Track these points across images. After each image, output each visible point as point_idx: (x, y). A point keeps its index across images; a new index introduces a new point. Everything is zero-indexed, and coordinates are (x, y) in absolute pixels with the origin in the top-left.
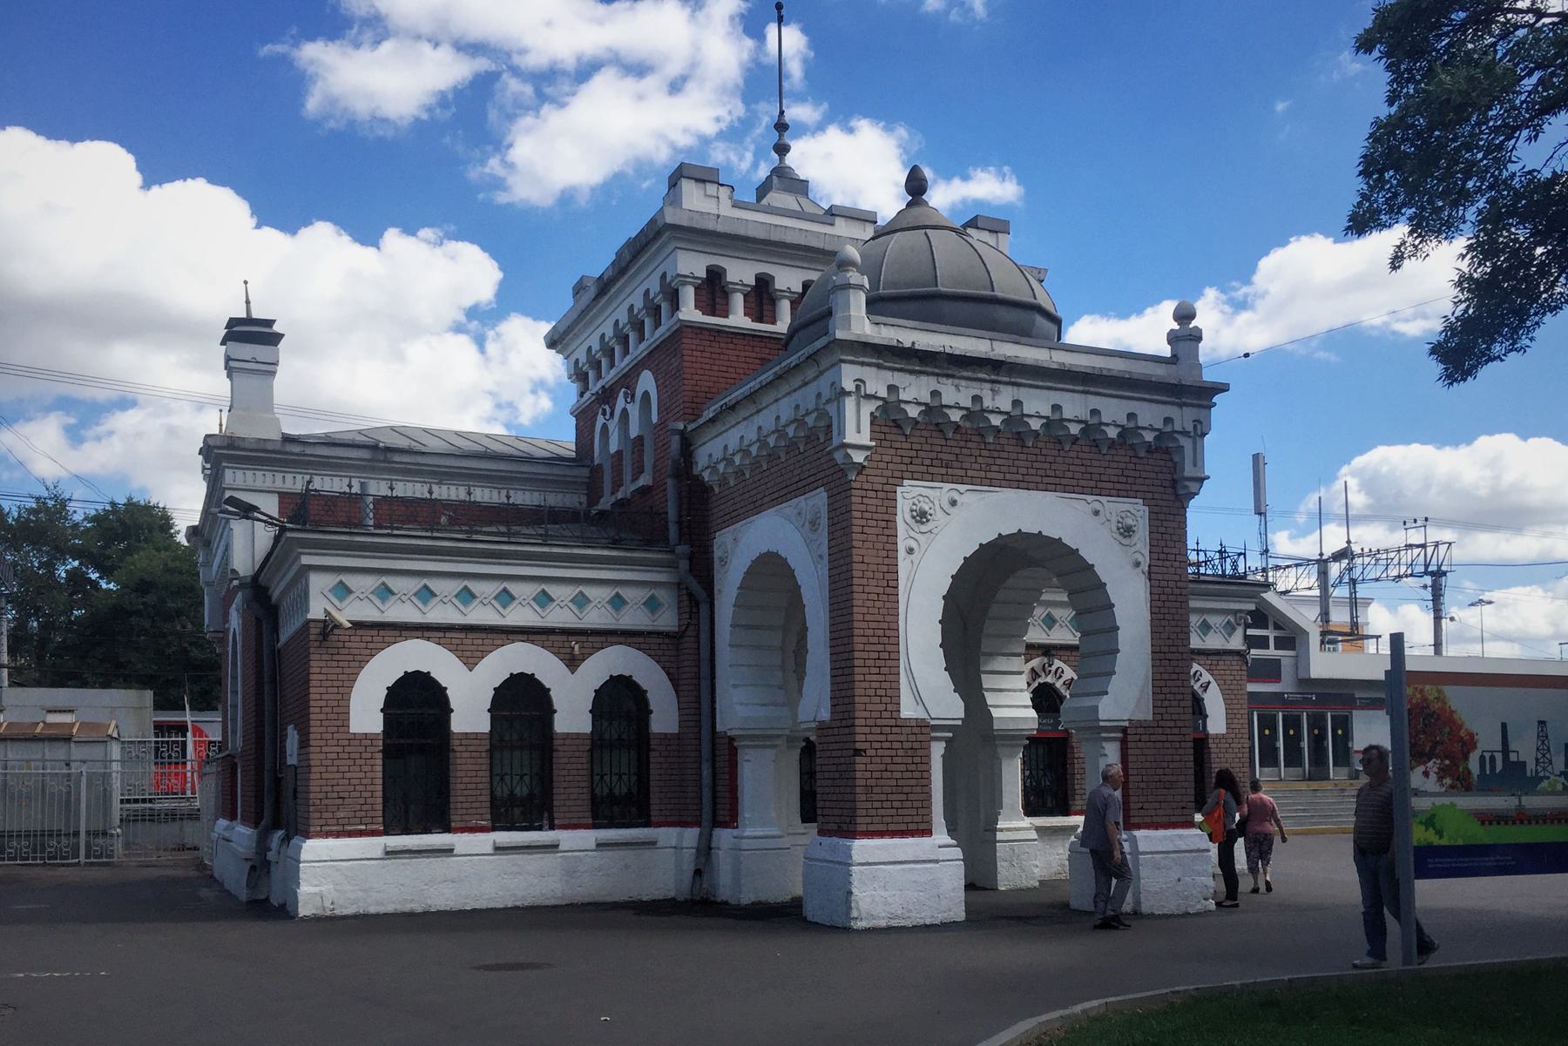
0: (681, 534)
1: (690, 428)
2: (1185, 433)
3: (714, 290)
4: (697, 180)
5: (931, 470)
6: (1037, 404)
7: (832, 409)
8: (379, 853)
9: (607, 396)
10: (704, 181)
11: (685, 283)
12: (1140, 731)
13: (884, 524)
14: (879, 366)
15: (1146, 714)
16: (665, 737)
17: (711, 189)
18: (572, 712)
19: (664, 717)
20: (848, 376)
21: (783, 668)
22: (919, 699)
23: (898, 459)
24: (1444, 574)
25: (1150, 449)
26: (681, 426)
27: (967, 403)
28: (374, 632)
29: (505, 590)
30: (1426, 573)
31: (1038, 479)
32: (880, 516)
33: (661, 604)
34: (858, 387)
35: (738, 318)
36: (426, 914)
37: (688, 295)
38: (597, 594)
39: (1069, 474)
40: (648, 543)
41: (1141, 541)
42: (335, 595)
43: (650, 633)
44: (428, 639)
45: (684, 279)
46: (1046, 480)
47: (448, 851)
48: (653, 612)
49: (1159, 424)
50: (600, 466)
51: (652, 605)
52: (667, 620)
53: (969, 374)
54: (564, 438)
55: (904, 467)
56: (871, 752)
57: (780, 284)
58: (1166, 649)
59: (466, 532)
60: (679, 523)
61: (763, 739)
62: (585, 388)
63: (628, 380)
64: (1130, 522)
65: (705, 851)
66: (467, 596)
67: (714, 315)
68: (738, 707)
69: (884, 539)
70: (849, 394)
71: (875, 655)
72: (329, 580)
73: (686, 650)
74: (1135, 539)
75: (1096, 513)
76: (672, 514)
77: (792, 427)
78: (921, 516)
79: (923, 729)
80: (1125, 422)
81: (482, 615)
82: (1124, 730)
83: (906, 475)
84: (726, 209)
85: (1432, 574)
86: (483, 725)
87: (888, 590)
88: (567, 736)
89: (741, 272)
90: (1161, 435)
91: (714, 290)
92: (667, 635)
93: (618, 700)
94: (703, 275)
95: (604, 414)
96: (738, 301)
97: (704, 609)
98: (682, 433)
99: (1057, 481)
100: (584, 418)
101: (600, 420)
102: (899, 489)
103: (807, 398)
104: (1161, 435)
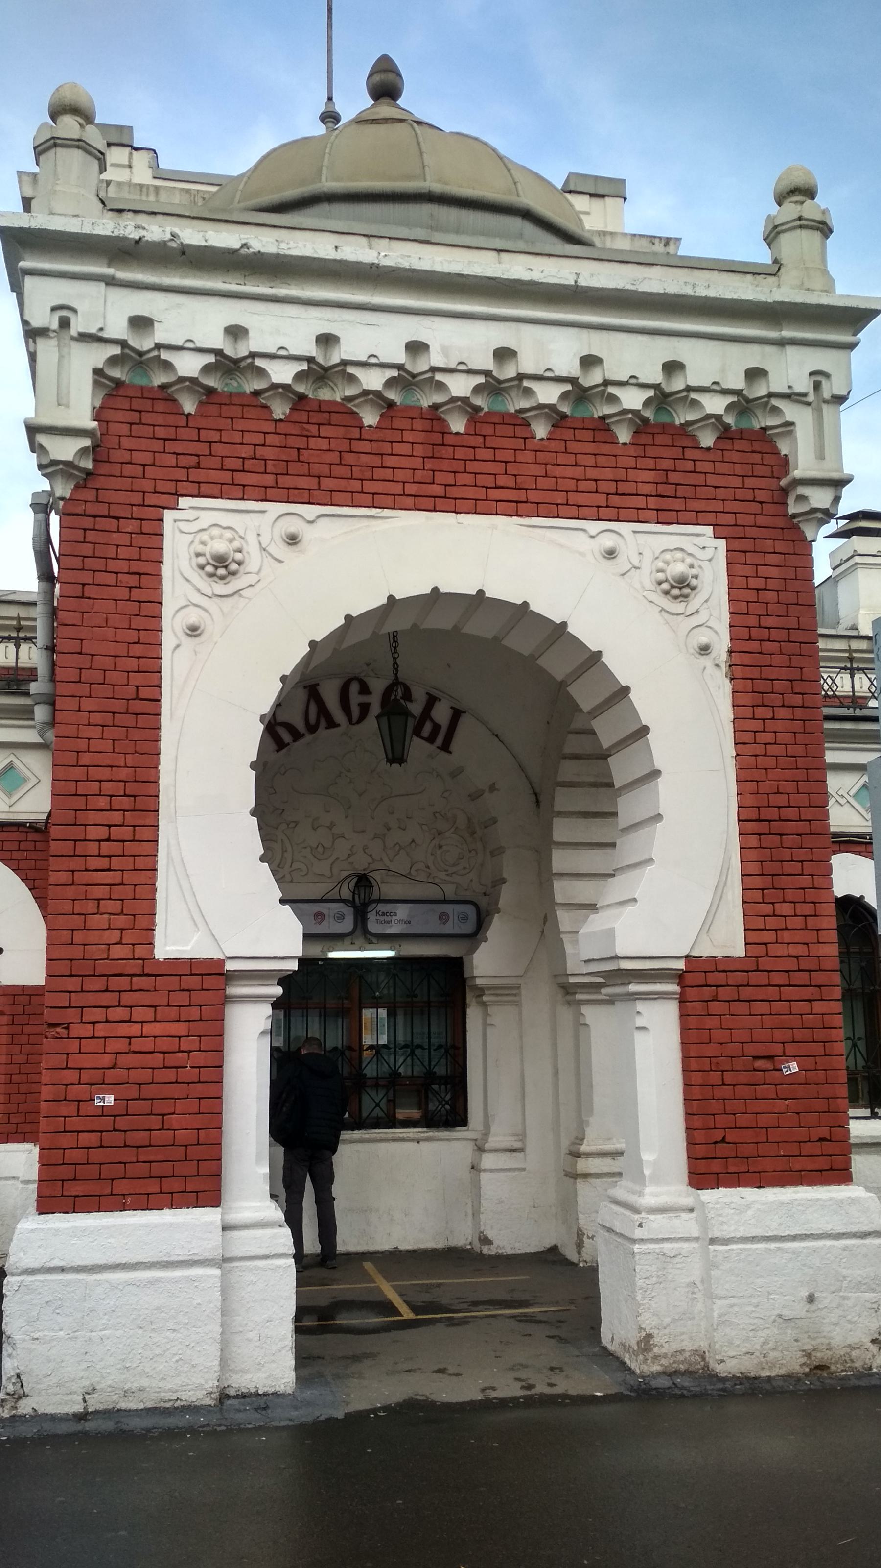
2: (791, 397)
5: (241, 478)
13: (133, 580)
14: (111, 282)
15: (729, 940)
23: (171, 460)
25: (641, 425)
27: (655, 376)
31: (481, 493)
32: (122, 566)
34: (817, 386)
39: (549, 483)
41: (713, 610)
42: (16, 787)
46: (495, 494)
49: (737, 382)
53: (263, 289)
55: (181, 474)
56: (77, 1030)
58: (772, 813)
64: (678, 568)
69: (133, 608)
71: (102, 832)
74: (696, 602)
75: (611, 554)
80: (489, 364)
83: (182, 487)
87: (137, 706)
90: (743, 405)
92: (31, 827)
99: (521, 495)
104: (743, 405)
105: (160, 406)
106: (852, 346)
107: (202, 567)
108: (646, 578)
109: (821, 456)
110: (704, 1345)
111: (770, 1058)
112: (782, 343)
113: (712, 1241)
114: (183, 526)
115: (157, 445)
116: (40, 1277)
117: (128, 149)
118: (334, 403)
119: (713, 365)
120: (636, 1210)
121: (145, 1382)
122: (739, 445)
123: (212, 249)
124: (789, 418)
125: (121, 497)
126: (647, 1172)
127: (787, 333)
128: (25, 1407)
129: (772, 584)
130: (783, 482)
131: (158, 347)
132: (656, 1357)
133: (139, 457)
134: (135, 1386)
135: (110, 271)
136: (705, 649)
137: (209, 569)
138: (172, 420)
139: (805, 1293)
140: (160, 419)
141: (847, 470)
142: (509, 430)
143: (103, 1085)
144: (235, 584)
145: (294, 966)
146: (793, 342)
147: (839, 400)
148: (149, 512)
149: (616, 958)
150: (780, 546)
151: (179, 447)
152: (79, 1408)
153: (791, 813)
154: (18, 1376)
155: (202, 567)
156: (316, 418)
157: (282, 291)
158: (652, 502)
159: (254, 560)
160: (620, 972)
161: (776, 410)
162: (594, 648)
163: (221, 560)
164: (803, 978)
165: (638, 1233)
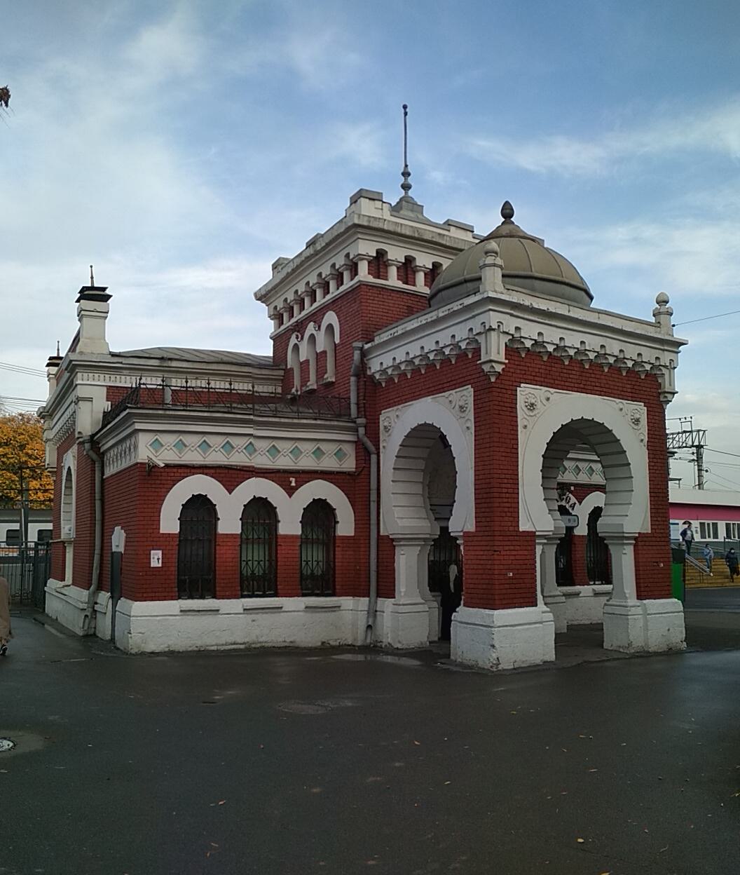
0: (359, 412)
1: (366, 346)
2: (665, 367)
3: (379, 263)
4: (370, 199)
6: (573, 340)
7: (481, 339)
8: (303, 607)
9: (300, 327)
10: (374, 200)
11: (363, 259)
12: (645, 539)
14: (512, 315)
15: (647, 529)
16: (345, 539)
17: (378, 204)
18: (290, 524)
19: (346, 525)
20: (493, 319)
21: (423, 495)
22: (530, 518)
23: (519, 371)
24: (702, 446)
25: (629, 370)
26: (360, 345)
28: (175, 470)
29: (318, 448)
30: (693, 446)
33: (345, 455)
34: (499, 326)
35: (393, 280)
36: (248, 649)
37: (363, 267)
38: (308, 447)
40: (338, 416)
43: (338, 473)
44: (206, 474)
45: (361, 257)
47: (279, 609)
48: (318, 458)
50: (292, 369)
51: (340, 454)
52: (349, 464)
54: (266, 350)
57: (419, 262)
59: (183, 406)
60: (358, 404)
61: (410, 540)
62: (281, 323)
63: (316, 317)
65: (373, 613)
66: (229, 447)
67: (379, 278)
68: (398, 521)
70: (494, 330)
72: (149, 438)
73: (359, 485)
75: (621, 409)
76: (353, 399)
77: (449, 349)
78: (532, 406)
79: (531, 536)
81: (238, 459)
82: (635, 539)
84: (387, 215)
85: (696, 446)
86: (297, 530)
88: (286, 537)
89: (396, 254)
91: (379, 263)
92: (349, 474)
93: (319, 513)
94: (375, 255)
95: (297, 338)
96: (393, 271)
97: (374, 457)
98: (361, 349)
100: (280, 341)
101: (293, 341)
102: (518, 389)
103: (461, 332)
105: (516, 354)
106: (678, 353)
107: (526, 406)
108: (629, 417)
109: (670, 385)
110: (644, 645)
111: (657, 562)
112: (664, 350)
113: (649, 614)
114: (522, 393)
115: (515, 367)
116: (501, 628)
117: (381, 203)
118: (557, 356)
119: (649, 355)
120: (626, 607)
121: (527, 658)
122: (650, 378)
123: (540, 309)
124: (663, 372)
125: (507, 383)
126: (627, 595)
127: (666, 348)
128: (500, 667)
129: (657, 421)
130: (660, 391)
131: (521, 337)
132: (633, 648)
133: (511, 370)
134: (524, 660)
135: (512, 312)
136: (642, 440)
137: (529, 407)
138: (519, 359)
139: (667, 628)
140: (516, 359)
141: (676, 390)
142: (598, 368)
143: (511, 570)
144: (535, 412)
145: (564, 536)
146: (667, 350)
147: (675, 368)
148: (514, 388)
149: (623, 533)
150: (659, 410)
151: (521, 368)
152: (512, 667)
153: (660, 491)
154: (498, 658)
155: (526, 406)
156: (554, 361)
157: (553, 323)
158: (631, 394)
159: (539, 405)
160: (623, 537)
161: (660, 370)
162: (618, 438)
163: (532, 405)
164: (663, 539)
165: (630, 613)
